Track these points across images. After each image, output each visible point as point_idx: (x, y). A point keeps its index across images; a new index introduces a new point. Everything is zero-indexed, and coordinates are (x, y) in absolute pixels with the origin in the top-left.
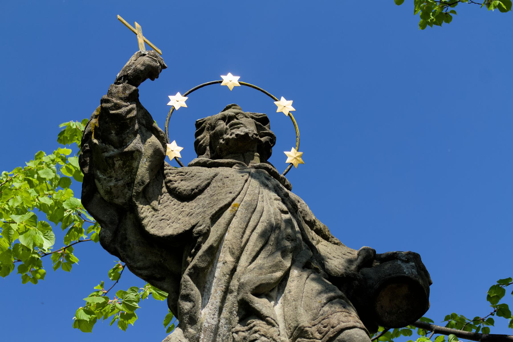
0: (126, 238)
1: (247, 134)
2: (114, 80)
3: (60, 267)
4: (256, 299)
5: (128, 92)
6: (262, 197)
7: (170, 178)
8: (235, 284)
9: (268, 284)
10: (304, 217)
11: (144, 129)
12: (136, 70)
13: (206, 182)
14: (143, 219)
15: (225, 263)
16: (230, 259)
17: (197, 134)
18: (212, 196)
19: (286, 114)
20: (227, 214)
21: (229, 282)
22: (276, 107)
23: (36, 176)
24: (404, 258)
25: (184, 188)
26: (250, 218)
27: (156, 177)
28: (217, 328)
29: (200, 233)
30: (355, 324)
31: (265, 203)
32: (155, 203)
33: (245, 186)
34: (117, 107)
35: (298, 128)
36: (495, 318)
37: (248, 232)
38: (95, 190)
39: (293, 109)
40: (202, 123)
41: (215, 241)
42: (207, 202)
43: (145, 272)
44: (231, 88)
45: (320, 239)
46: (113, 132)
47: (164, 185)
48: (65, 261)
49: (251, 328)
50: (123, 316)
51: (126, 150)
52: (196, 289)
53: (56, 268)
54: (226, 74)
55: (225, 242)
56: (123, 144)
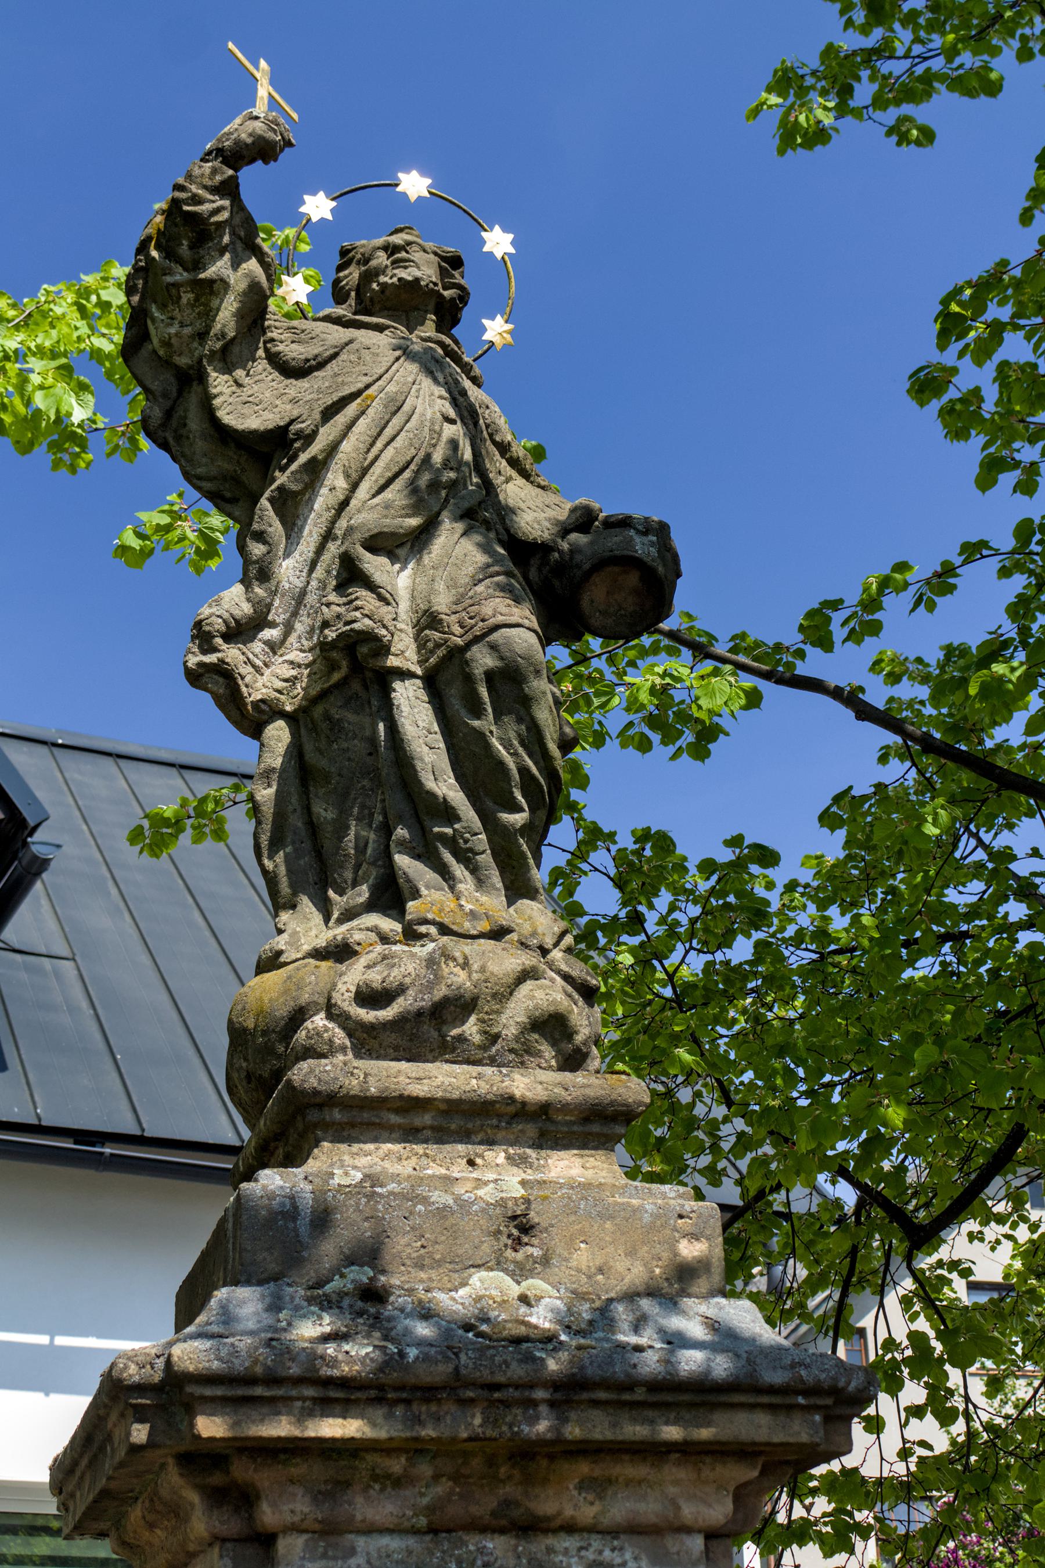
0: (185, 425)
1: (417, 280)
2: (201, 155)
3: (117, 455)
4: (367, 556)
5: (218, 178)
6: (418, 391)
7: (274, 334)
8: (342, 524)
9: (393, 534)
10: (491, 435)
11: (239, 246)
12: (237, 142)
13: (332, 351)
14: (215, 396)
15: (332, 489)
16: (341, 483)
17: (340, 268)
18: (336, 375)
19: (499, 256)
20: (352, 409)
21: (333, 522)
22: (483, 242)
23: (94, 298)
24: (640, 528)
25: (294, 355)
26: (388, 422)
27: (249, 330)
28: (303, 593)
29: (299, 434)
30: (520, 621)
31: (420, 400)
32: (240, 373)
33: (394, 368)
34: (196, 200)
35: (513, 284)
36: (808, 648)
37: (379, 445)
38: (146, 337)
39: (512, 250)
40: (349, 251)
41: (322, 451)
42: (327, 384)
43: (207, 485)
44: (413, 197)
45: (514, 473)
46: (185, 242)
47: (261, 345)
48: (128, 445)
49: (351, 602)
50: (198, 551)
51: (202, 276)
52: (277, 525)
53: (110, 455)
54: (407, 171)
55: (340, 455)
56: (198, 265)
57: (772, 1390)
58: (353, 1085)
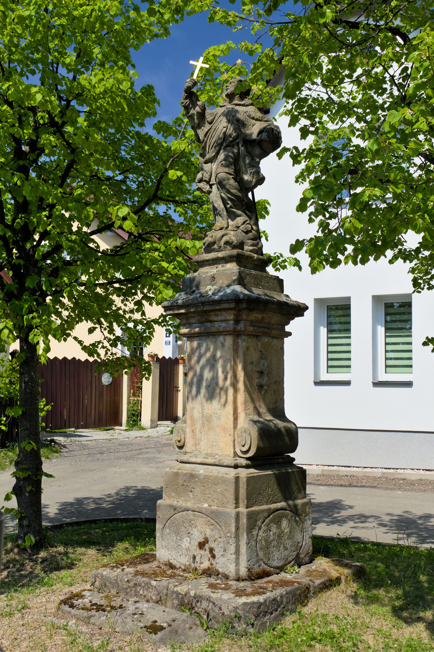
57: (225, 301)
58: (207, 258)
